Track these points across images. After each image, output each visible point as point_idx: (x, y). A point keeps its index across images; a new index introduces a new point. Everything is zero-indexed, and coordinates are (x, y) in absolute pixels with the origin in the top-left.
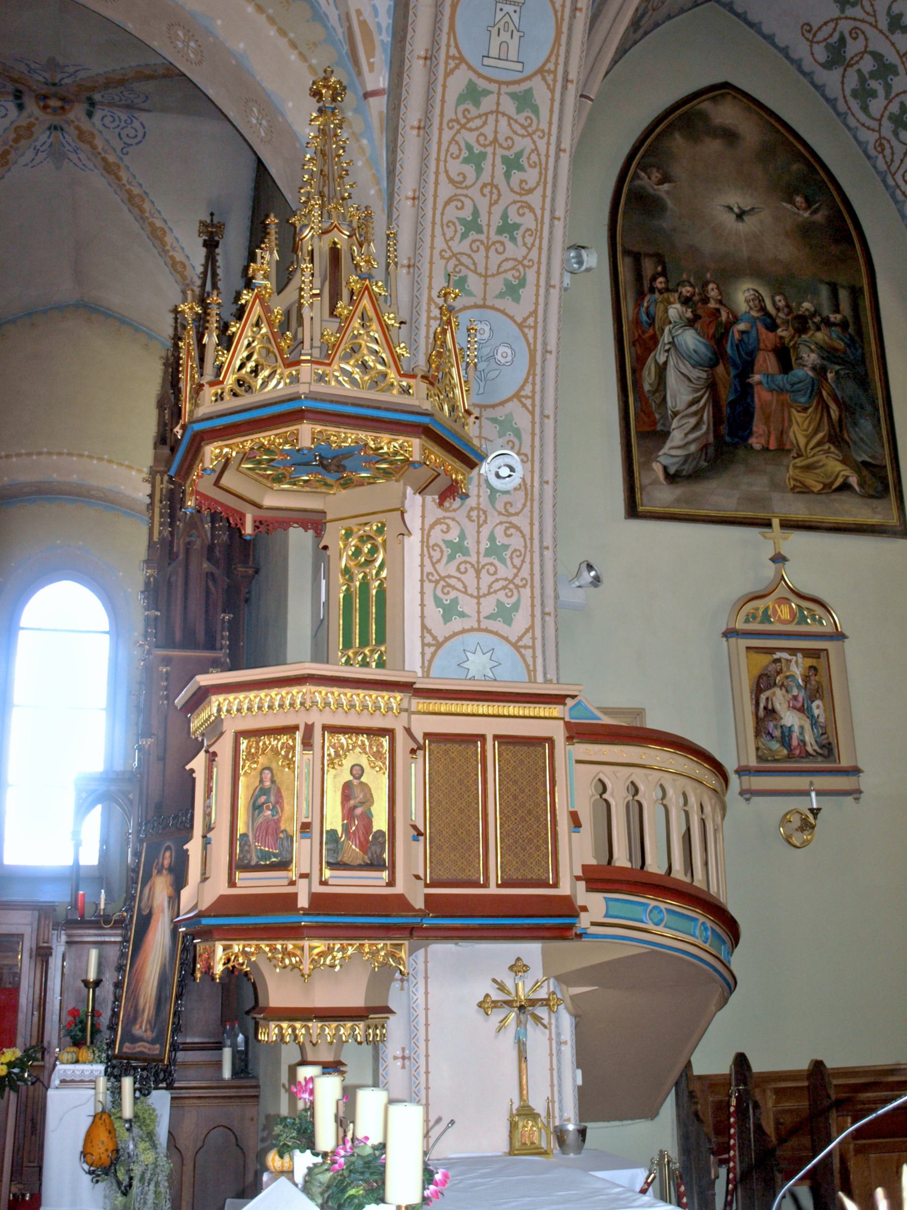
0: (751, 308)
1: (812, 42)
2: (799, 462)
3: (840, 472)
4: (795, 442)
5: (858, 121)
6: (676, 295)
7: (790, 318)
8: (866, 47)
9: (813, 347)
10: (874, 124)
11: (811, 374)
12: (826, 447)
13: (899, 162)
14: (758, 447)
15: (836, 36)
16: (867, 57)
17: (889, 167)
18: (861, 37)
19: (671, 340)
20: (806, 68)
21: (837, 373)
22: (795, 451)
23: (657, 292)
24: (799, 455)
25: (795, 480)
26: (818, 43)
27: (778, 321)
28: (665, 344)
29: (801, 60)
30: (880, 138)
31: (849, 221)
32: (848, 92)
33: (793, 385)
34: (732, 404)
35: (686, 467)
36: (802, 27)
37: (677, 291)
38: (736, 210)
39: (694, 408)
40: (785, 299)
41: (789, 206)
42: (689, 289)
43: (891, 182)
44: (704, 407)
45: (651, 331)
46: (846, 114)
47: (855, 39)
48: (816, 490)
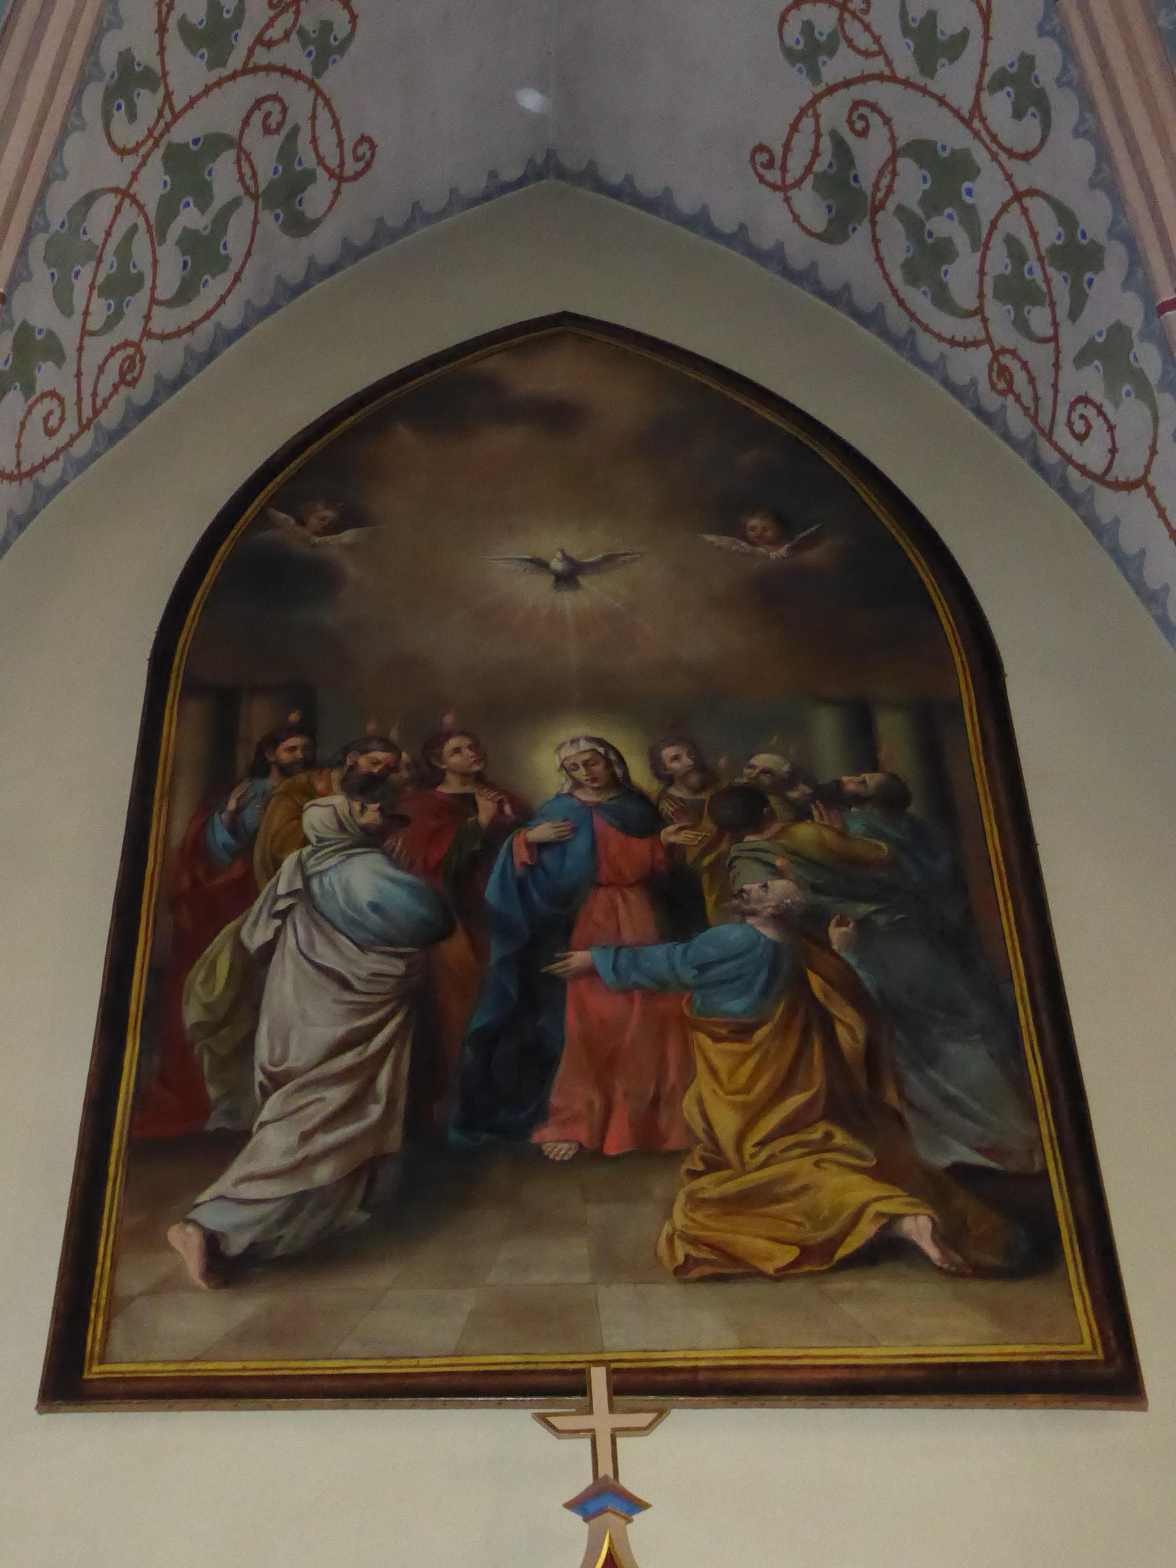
0: (578, 784)
1: (781, 188)
2: (711, 1186)
3: (864, 1206)
4: (698, 1126)
5: (940, 337)
6: (336, 775)
7: (705, 796)
8: (893, 139)
9: (779, 862)
10: (970, 328)
11: (769, 933)
12: (817, 1134)
13: (1051, 392)
14: (561, 1150)
15: (826, 144)
16: (905, 165)
17: (1035, 419)
18: (875, 119)
19: (299, 884)
20: (798, 262)
21: (863, 923)
22: (698, 1151)
23: (275, 773)
24: (715, 1163)
25: (694, 1241)
26: (798, 183)
27: (666, 808)
28: (277, 898)
29: (780, 247)
30: (996, 354)
31: (913, 554)
33: (702, 968)
34: (487, 1039)
35: (289, 1232)
37: (342, 763)
38: (557, 565)
39: (348, 1059)
40: (695, 751)
41: (724, 541)
42: (380, 755)
43: (1051, 457)
44: (379, 1058)
45: (238, 869)
46: (912, 332)
47: (863, 133)
48: (769, 1268)
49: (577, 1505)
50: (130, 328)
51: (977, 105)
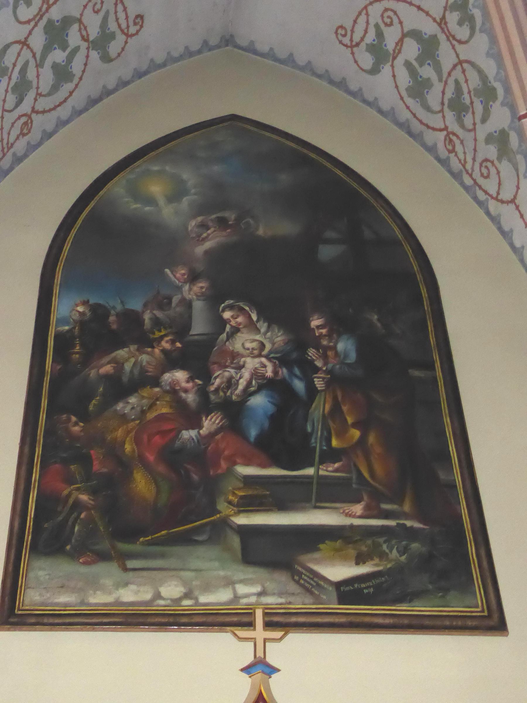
17: (464, 166)
32: (404, 94)
36: (336, 33)
49: (246, 670)
50: (26, 107)
51: (444, 17)
